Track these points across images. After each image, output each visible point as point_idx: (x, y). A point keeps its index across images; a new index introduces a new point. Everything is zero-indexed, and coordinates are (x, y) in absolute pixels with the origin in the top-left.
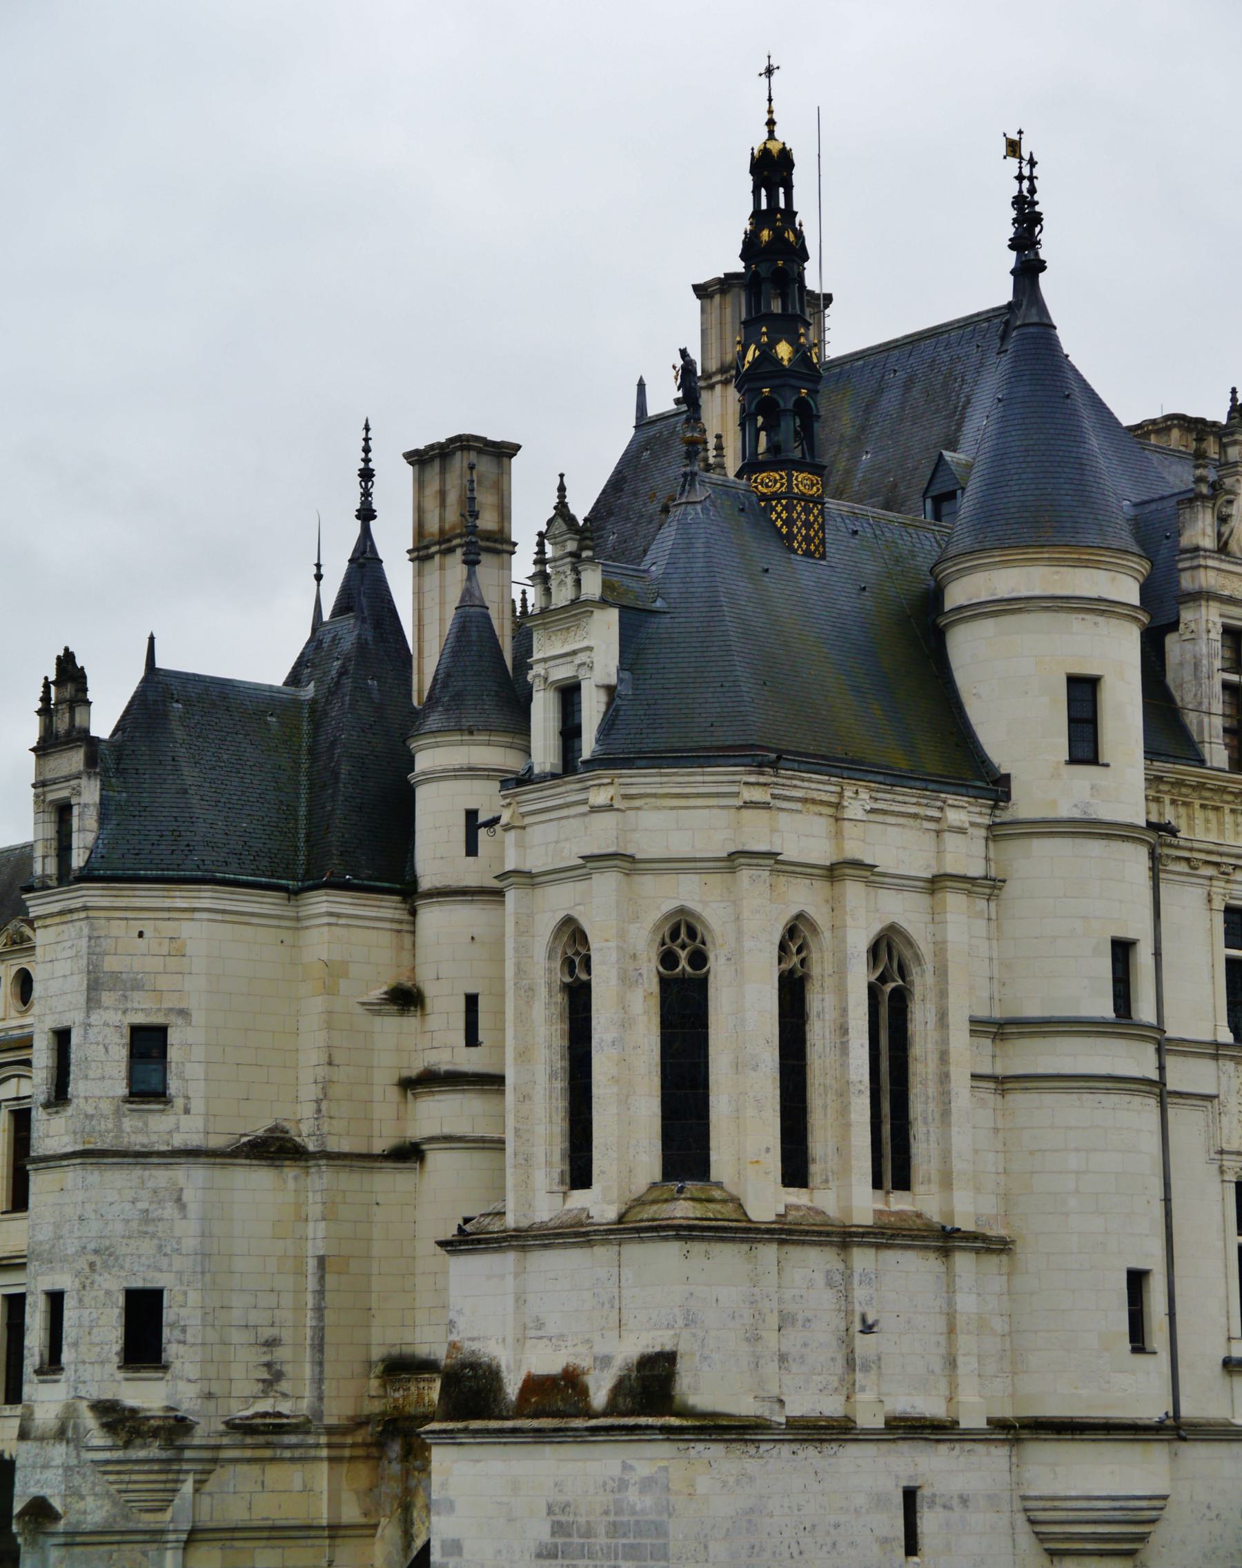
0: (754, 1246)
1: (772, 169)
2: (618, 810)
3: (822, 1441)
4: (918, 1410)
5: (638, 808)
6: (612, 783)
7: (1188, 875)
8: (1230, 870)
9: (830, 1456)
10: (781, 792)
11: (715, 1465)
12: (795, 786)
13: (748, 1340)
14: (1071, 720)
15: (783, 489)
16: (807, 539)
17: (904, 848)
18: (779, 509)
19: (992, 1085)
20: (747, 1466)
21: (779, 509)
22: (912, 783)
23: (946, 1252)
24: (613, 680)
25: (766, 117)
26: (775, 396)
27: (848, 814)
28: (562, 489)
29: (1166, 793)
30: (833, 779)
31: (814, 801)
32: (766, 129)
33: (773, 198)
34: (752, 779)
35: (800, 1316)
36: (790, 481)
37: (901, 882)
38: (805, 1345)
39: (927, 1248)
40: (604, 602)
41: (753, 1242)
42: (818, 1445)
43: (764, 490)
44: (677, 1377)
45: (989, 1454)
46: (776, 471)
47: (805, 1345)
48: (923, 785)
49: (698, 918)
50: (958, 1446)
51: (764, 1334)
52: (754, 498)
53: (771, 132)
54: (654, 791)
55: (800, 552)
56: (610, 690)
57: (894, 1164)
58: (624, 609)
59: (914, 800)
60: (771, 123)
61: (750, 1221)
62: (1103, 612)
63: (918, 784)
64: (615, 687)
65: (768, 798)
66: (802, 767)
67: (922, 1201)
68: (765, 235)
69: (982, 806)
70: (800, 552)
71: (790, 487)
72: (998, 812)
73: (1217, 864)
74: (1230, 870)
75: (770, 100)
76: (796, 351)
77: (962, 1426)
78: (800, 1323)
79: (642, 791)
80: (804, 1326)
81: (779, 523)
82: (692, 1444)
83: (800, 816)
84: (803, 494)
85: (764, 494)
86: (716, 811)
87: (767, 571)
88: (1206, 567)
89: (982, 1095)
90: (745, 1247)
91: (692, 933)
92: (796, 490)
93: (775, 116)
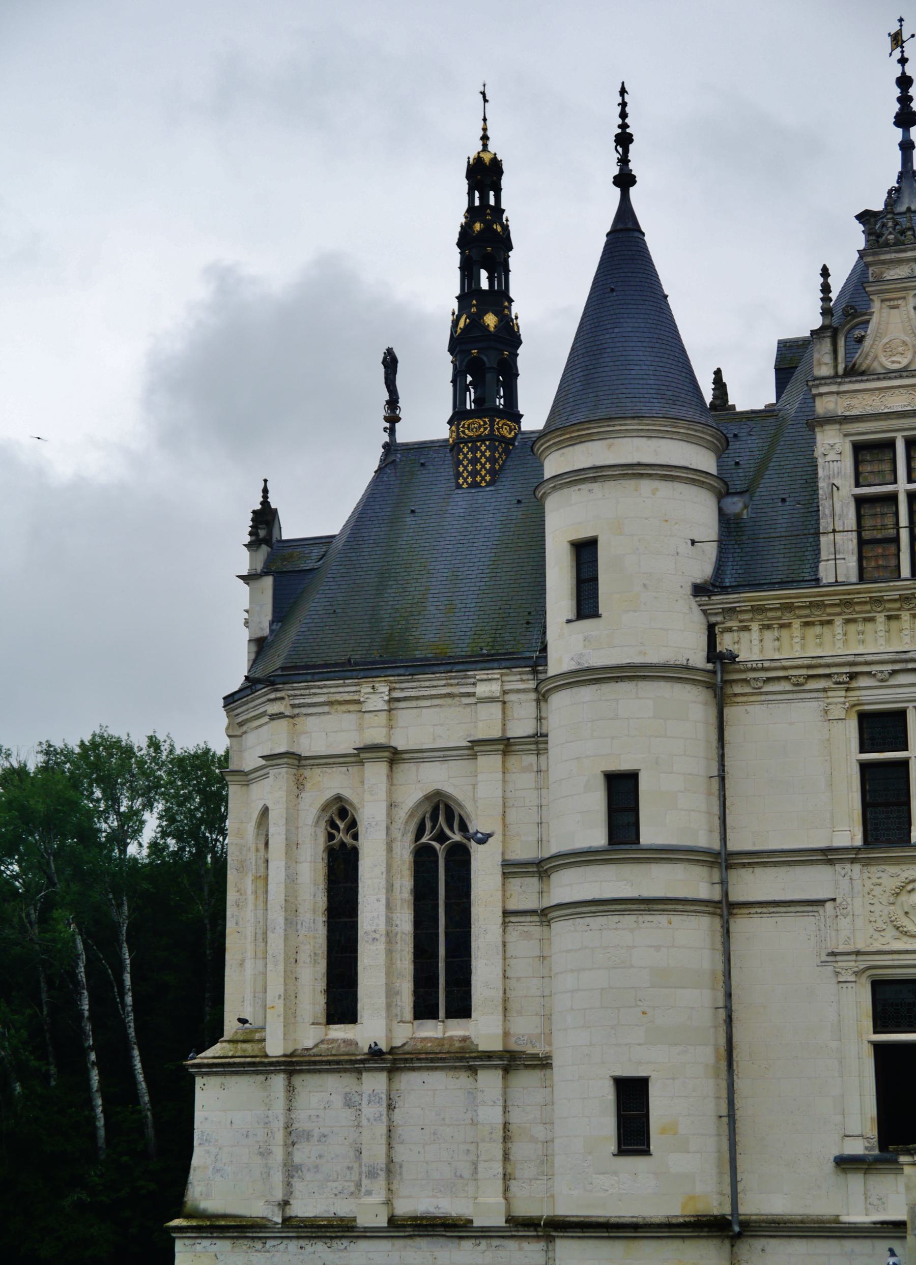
0: (269, 1076)
1: (485, 175)
3: (331, 1238)
4: (442, 1211)
7: (792, 692)
9: (342, 1251)
10: (302, 701)
11: (220, 1257)
12: (315, 694)
13: (261, 1154)
15: (486, 432)
17: (442, 725)
18: (465, 450)
19: (536, 918)
20: (252, 1258)
21: (465, 450)
22: (436, 669)
23: (473, 1070)
25: (481, 133)
27: (368, 706)
28: (265, 491)
29: (752, 620)
30: (347, 681)
31: (340, 703)
32: (481, 143)
33: (484, 198)
35: (316, 1133)
36: (492, 425)
37: (443, 754)
38: (320, 1156)
39: (455, 1068)
41: (269, 1074)
42: (328, 1241)
44: (190, 1186)
45: (521, 1249)
46: (480, 418)
47: (320, 1156)
48: (449, 668)
49: (449, 797)
50: (484, 1242)
51: (274, 1149)
53: (485, 146)
55: (465, 486)
59: (443, 682)
60: (485, 138)
61: (267, 1056)
62: (594, 479)
63: (442, 668)
66: (316, 677)
67: (483, 1029)
68: (478, 226)
69: (521, 673)
70: (465, 486)
71: (492, 430)
73: (828, 676)
74: (801, 680)
75: (485, 120)
76: (500, 321)
77: (475, 1224)
78: (316, 1138)
80: (319, 1141)
82: (199, 1241)
84: (470, 437)
88: (821, 395)
89: (525, 929)
90: (261, 1078)
91: (450, 815)
93: (489, 133)
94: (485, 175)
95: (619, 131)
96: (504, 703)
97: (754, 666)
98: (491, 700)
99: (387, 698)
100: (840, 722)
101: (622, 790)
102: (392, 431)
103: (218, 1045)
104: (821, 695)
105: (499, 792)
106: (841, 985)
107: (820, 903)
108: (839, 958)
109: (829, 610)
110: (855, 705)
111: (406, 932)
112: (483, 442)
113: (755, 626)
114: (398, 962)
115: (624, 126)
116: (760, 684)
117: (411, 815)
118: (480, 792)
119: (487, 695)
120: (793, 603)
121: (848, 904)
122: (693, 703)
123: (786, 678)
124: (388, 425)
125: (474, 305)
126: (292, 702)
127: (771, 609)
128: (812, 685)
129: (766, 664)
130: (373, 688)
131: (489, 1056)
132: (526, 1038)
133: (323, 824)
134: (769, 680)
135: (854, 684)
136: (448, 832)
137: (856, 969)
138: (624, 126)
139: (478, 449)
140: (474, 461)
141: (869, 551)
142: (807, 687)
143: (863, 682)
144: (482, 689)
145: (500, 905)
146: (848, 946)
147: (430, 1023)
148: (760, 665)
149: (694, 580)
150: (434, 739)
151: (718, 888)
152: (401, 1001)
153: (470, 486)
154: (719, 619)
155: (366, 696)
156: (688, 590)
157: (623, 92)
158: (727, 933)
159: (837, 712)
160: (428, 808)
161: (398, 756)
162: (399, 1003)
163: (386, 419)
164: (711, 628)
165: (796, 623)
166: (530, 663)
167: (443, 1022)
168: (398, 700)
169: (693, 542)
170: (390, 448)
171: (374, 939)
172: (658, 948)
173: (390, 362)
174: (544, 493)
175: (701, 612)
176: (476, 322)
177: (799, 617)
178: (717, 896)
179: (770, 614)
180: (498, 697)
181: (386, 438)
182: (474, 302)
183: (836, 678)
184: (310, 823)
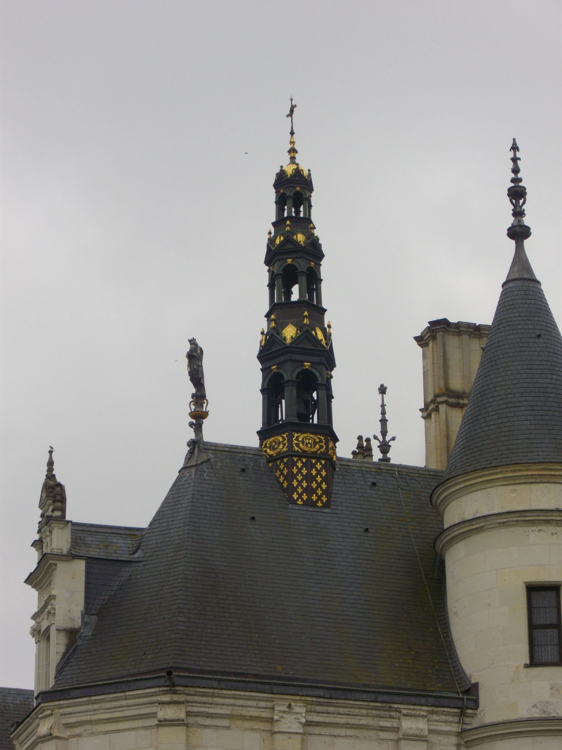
1: (293, 190)
2: (56, 737)
5: (79, 736)
6: (51, 714)
14: (532, 627)
16: (309, 491)
24: (78, 623)
26: (281, 371)
27: (282, 726)
28: (51, 464)
31: (243, 718)
34: (166, 698)
40: (72, 556)
43: (271, 453)
46: (315, 434)
48: (373, 697)
52: (263, 461)
54: (88, 718)
55: (300, 502)
56: (72, 634)
58: (90, 561)
63: (364, 696)
64: (78, 630)
65: (182, 715)
69: (448, 714)
71: (290, 446)
72: (467, 720)
75: (517, 193)
79: (79, 719)
81: (282, 479)
83: (228, 732)
84: (305, 452)
85: (271, 456)
86: (142, 732)
87: (253, 518)
92: (296, 449)
94: (293, 190)
95: (512, 185)
99: (304, 720)
102: (197, 427)
112: (318, 459)
115: (516, 180)
119: (413, 732)
124: (194, 421)
125: (288, 225)
130: (290, 706)
138: (516, 180)
139: (314, 466)
140: (309, 478)
141: (537, 633)
144: (409, 725)
153: (306, 503)
155: (280, 714)
157: (515, 148)
163: (192, 415)
166: (460, 704)
168: (317, 724)
170: (196, 445)
173: (195, 356)
174: (482, 527)
176: (289, 240)
181: (191, 434)
182: (306, 313)
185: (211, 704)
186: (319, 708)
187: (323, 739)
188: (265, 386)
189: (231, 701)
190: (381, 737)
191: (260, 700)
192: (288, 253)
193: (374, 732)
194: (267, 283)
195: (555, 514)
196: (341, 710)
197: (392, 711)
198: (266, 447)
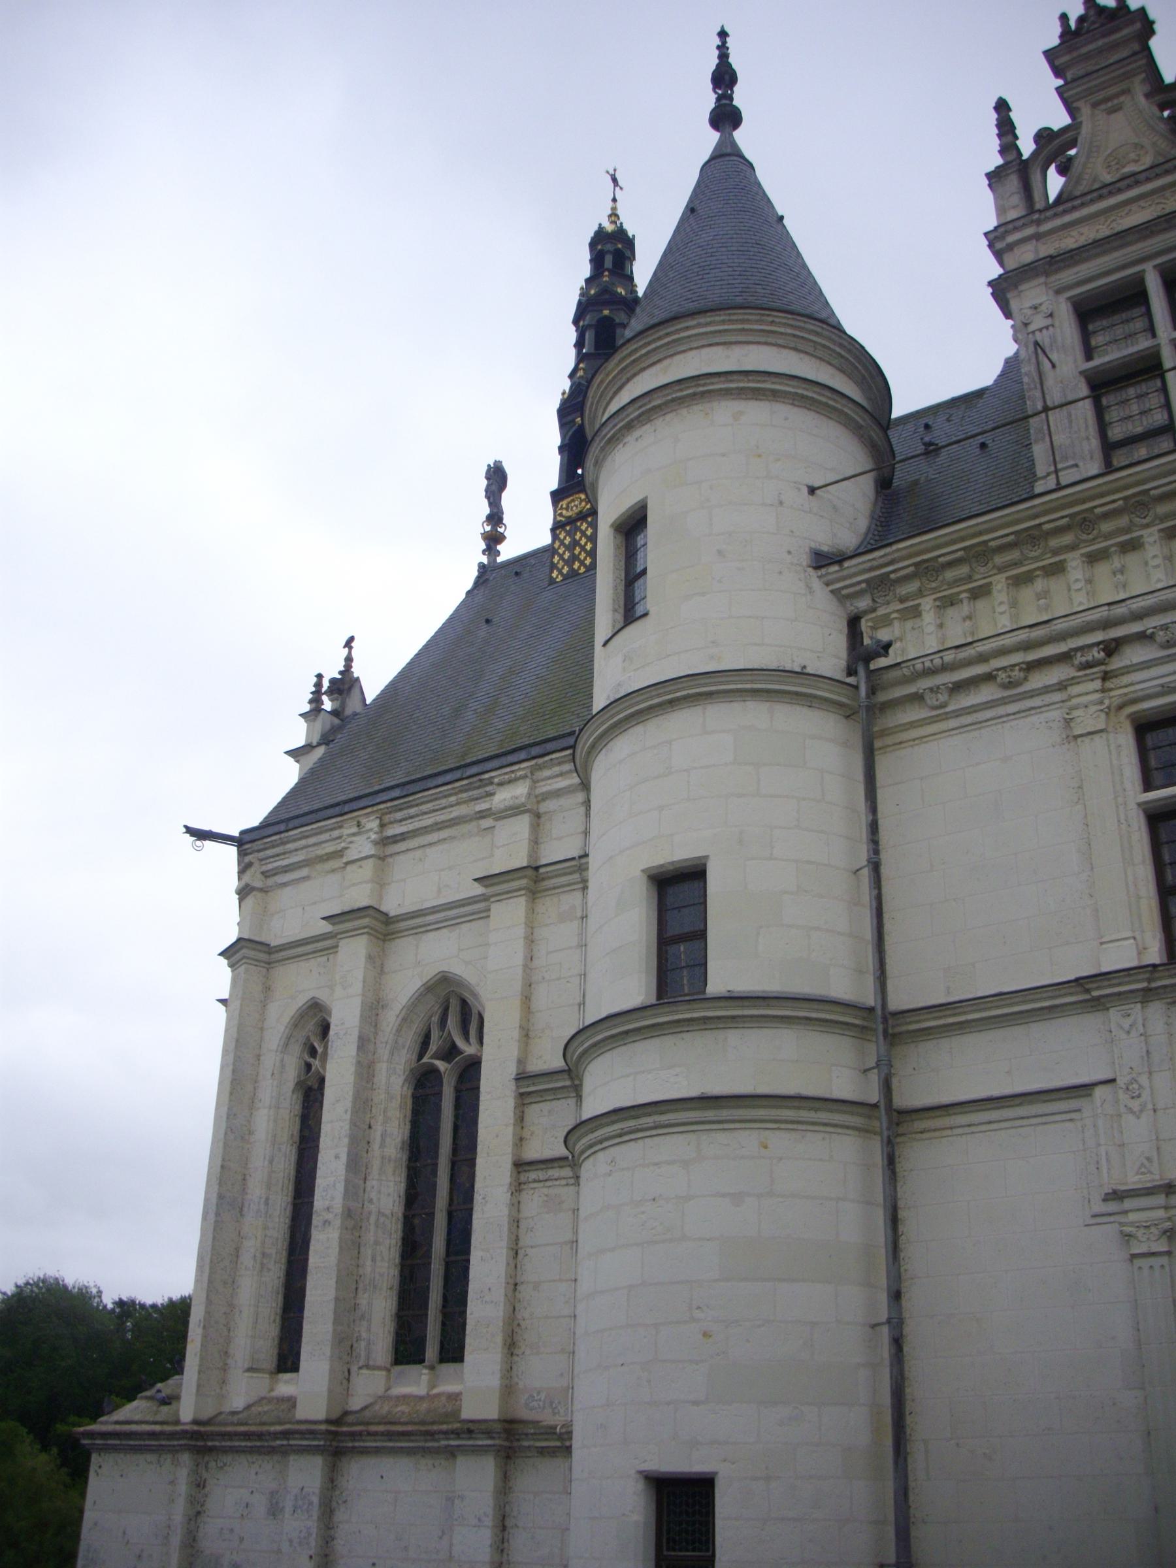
7: (1003, 701)
8: (1017, 674)
25: (711, 61)
27: (352, 854)
29: (920, 593)
57: (428, 1320)
74: (1017, 674)
83: (307, 884)
96: (538, 816)
97: (928, 664)
98: (514, 811)
100: (1096, 737)
101: (678, 890)
103: (135, 1403)
104: (1057, 697)
105: (519, 959)
106: (1138, 1262)
107: (1083, 1090)
108: (1128, 1204)
109: (1054, 543)
110: (1120, 707)
111: (388, 1212)
113: (927, 603)
114: (369, 1263)
116: (943, 698)
117: (405, 1020)
118: (487, 957)
120: (985, 542)
121: (1141, 1087)
122: (816, 746)
123: (989, 677)
126: (264, 868)
127: (950, 564)
128: (1038, 680)
129: (949, 657)
131: (471, 1429)
132: (543, 1396)
133: (296, 1049)
134: (958, 688)
135: (1116, 663)
136: (460, 1043)
137: (1168, 1225)
141: (1150, 739)
142: (1027, 687)
143: (1134, 655)
144: (503, 797)
145: (509, 1149)
146: (1148, 1177)
147: (412, 1370)
148: (938, 662)
149: (813, 545)
150: (439, 891)
151: (874, 1078)
152: (369, 1330)
154: (863, 603)
156: (805, 560)
158: (891, 1161)
159: (1088, 720)
160: (432, 1005)
161: (392, 927)
162: (364, 1335)
164: (854, 623)
165: (999, 583)
167: (432, 1368)
168: (403, 837)
169: (812, 490)
171: (326, 1221)
172: (737, 1198)
175: (831, 596)
177: (1001, 569)
178: (873, 1095)
179: (949, 575)
180: (523, 805)
183: (1079, 659)
184: (275, 1047)
185: (284, 853)
186: (399, 815)
187: (410, 855)
188: (567, 441)
189: (303, 842)
190: (483, 827)
191: (332, 830)
192: (606, 304)
193: (474, 823)
194: (574, 341)
195: (630, 410)
196: (424, 808)
197: (486, 785)
198: (562, 508)
